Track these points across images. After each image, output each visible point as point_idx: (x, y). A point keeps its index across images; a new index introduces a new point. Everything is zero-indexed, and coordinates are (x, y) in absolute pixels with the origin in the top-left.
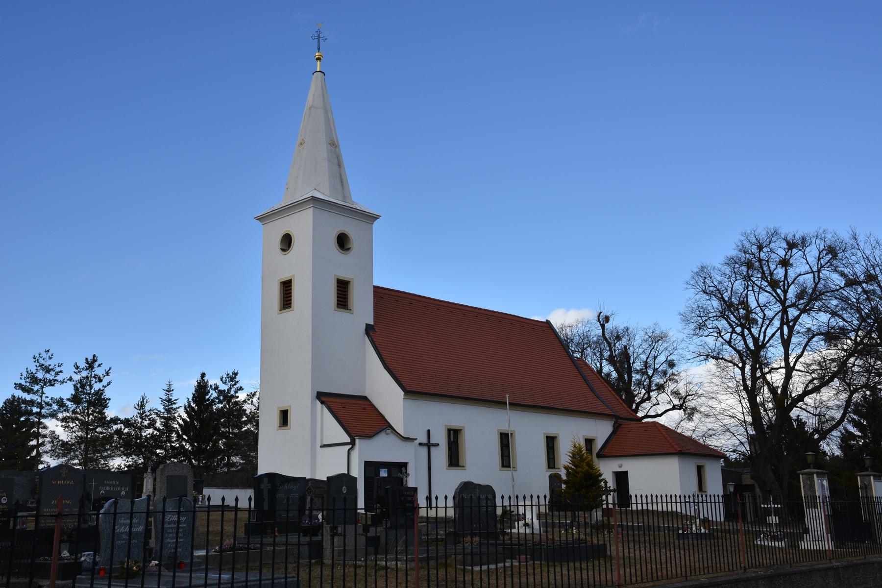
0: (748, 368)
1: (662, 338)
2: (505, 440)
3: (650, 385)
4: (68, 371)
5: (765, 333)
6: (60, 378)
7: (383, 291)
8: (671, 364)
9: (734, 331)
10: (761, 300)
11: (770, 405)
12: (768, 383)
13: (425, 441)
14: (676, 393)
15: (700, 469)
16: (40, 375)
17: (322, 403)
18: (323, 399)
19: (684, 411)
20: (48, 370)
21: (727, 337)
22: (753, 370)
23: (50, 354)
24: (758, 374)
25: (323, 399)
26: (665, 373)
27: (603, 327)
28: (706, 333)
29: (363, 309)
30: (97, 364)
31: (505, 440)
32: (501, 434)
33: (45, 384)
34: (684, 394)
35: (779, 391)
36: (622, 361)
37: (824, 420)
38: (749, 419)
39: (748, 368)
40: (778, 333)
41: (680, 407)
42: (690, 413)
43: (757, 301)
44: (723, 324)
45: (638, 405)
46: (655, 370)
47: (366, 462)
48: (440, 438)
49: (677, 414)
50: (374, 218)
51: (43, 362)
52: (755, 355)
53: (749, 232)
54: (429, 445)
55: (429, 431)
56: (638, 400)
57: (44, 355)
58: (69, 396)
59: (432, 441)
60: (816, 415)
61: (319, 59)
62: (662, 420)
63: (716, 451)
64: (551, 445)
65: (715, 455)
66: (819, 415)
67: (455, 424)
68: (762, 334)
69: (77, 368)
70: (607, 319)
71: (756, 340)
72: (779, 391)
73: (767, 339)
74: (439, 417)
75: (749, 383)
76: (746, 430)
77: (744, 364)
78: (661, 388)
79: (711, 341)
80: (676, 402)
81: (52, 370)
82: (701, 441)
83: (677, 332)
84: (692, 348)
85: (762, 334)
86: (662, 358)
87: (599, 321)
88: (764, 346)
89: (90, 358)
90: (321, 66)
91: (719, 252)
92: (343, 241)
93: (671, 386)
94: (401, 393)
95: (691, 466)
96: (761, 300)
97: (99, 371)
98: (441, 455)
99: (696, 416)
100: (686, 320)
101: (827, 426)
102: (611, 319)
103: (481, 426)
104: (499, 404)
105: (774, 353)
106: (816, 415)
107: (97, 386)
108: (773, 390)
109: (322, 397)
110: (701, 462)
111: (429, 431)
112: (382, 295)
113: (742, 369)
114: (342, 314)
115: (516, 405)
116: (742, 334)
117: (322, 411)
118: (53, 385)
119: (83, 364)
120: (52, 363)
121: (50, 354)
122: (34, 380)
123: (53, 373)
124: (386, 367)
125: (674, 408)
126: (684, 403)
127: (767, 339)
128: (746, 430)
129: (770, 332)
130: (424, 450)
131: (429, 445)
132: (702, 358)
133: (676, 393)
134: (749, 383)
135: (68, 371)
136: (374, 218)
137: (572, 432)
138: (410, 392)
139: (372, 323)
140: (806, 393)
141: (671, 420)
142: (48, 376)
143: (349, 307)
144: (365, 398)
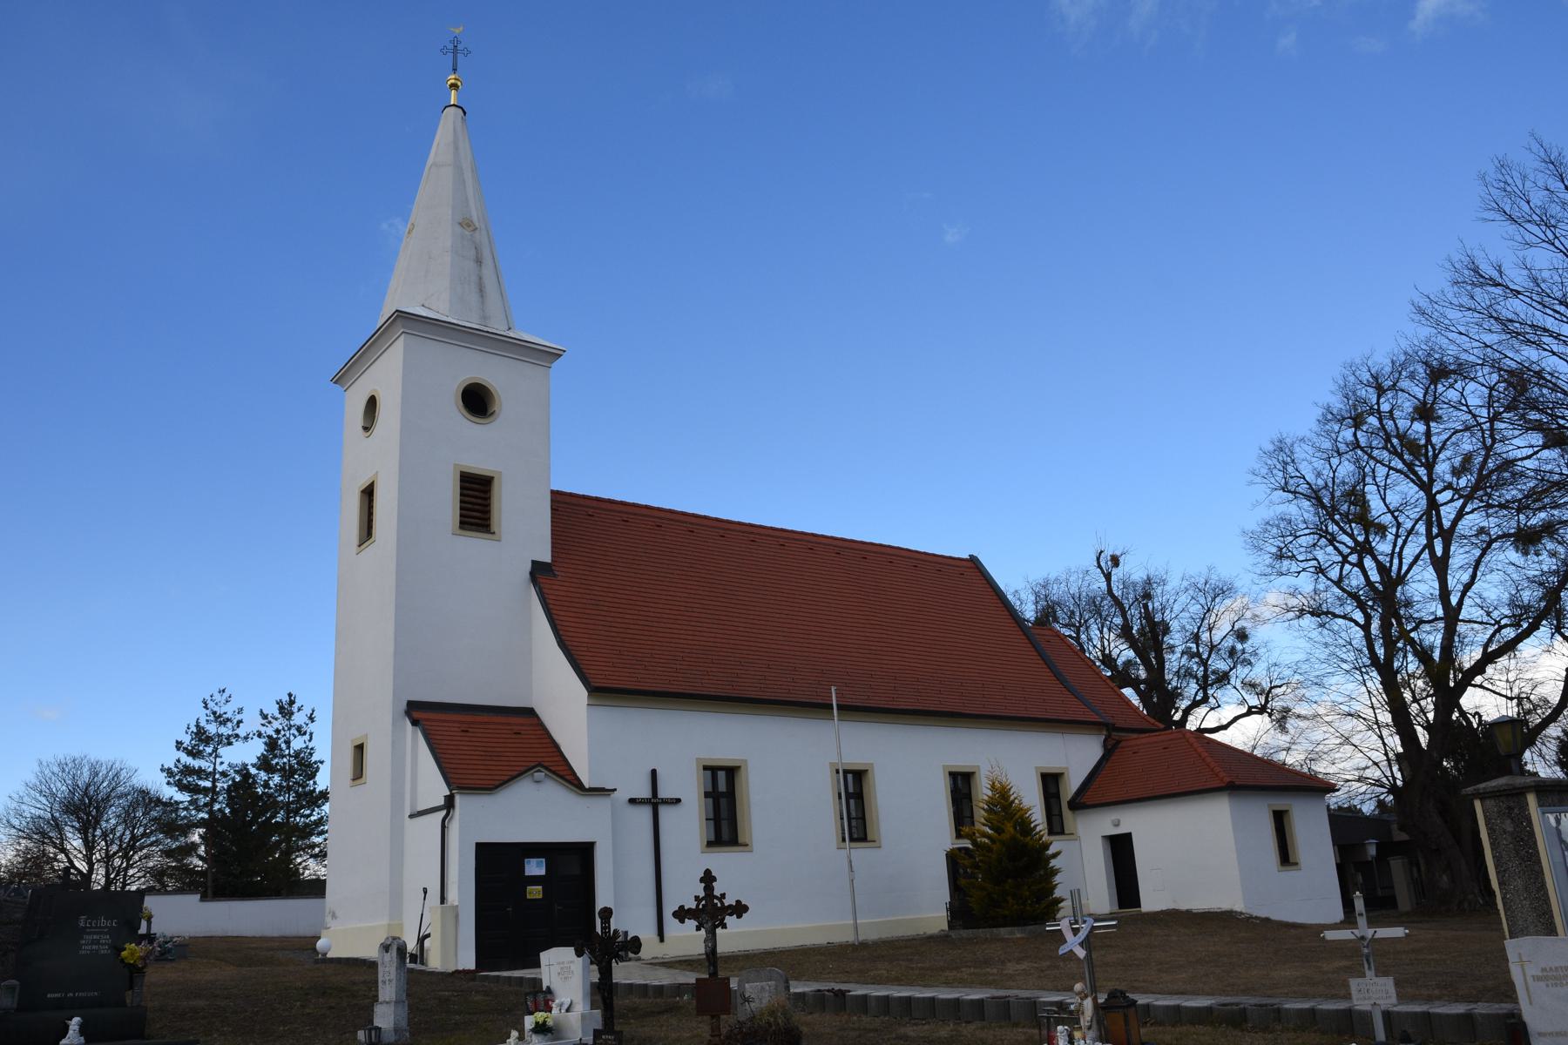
0: (1375, 625)
1: (1222, 591)
2: (854, 787)
3: (1206, 676)
4: (252, 723)
5: (1395, 545)
6: (241, 731)
7: (595, 504)
8: (1242, 636)
9: (1345, 560)
10: (1395, 495)
11: (1420, 683)
12: (1412, 642)
13: (645, 793)
14: (1252, 686)
15: (1280, 818)
16: (212, 729)
17: (415, 723)
18: (416, 715)
19: (1270, 715)
20: (220, 719)
21: (1334, 573)
22: (1385, 627)
23: (226, 695)
24: (1394, 631)
25: (416, 715)
26: (1232, 652)
27: (1108, 577)
28: (1294, 568)
29: (526, 532)
30: (295, 707)
31: (854, 787)
32: (951, 774)
33: (220, 742)
34: (1266, 686)
35: (1436, 655)
36: (1150, 638)
37: (1527, 706)
38: (1386, 717)
39: (1375, 625)
40: (1426, 555)
41: (1262, 710)
42: (1282, 719)
43: (1384, 500)
44: (1326, 555)
45: (1187, 712)
46: (1213, 648)
47: (480, 847)
48: (686, 785)
49: (1259, 722)
50: (555, 355)
51: (216, 709)
52: (1385, 597)
53: (1358, 361)
54: (655, 803)
55: (654, 772)
56: (1184, 704)
57: (217, 697)
58: (255, 761)
59: (662, 794)
60: (1511, 699)
61: (454, 86)
62: (1218, 737)
63: (1321, 781)
64: (1052, 790)
65: (1316, 787)
66: (1519, 699)
67: (724, 754)
68: (1396, 561)
69: (265, 717)
70: (1115, 561)
71: (1383, 570)
72: (1436, 655)
73: (1405, 568)
74: (679, 743)
75: (1380, 652)
76: (1381, 737)
77: (1368, 618)
78: (1223, 679)
79: (1306, 583)
80: (1254, 701)
81: (228, 720)
82: (1305, 770)
83: (1239, 564)
84: (1273, 598)
85: (1396, 561)
86: (1223, 628)
87: (1099, 566)
88: (1401, 579)
89: (285, 699)
90: (458, 98)
91: (1297, 406)
92: (477, 401)
93: (1242, 671)
94: (582, 692)
95: (1259, 813)
96: (1395, 495)
97: (299, 719)
98: (686, 825)
99: (1291, 723)
100: (1255, 542)
101: (1535, 720)
102: (1121, 560)
103: (794, 764)
104: (816, 707)
105: (1421, 585)
106: (1511, 699)
107: (298, 743)
108: (1423, 655)
109: (417, 712)
110: (1280, 803)
111: (654, 772)
112: (566, 508)
113: (1366, 628)
114: (474, 543)
115: (851, 710)
116: (1360, 565)
117: (415, 741)
118: (230, 744)
119: (273, 710)
120: (228, 710)
121: (226, 695)
122: (201, 735)
123: (229, 725)
124: (562, 644)
125: (1249, 713)
126: (1267, 701)
127: (1405, 568)
128: (1381, 737)
129: (1410, 552)
130: (645, 813)
131: (655, 803)
132: (1291, 615)
133: (1252, 686)
134: (1380, 652)
135: (252, 723)
136: (555, 355)
137: (1015, 762)
138: (601, 691)
139: (547, 558)
140: (1488, 658)
141: (1248, 734)
142: (224, 730)
143: (494, 528)
144: (530, 712)
